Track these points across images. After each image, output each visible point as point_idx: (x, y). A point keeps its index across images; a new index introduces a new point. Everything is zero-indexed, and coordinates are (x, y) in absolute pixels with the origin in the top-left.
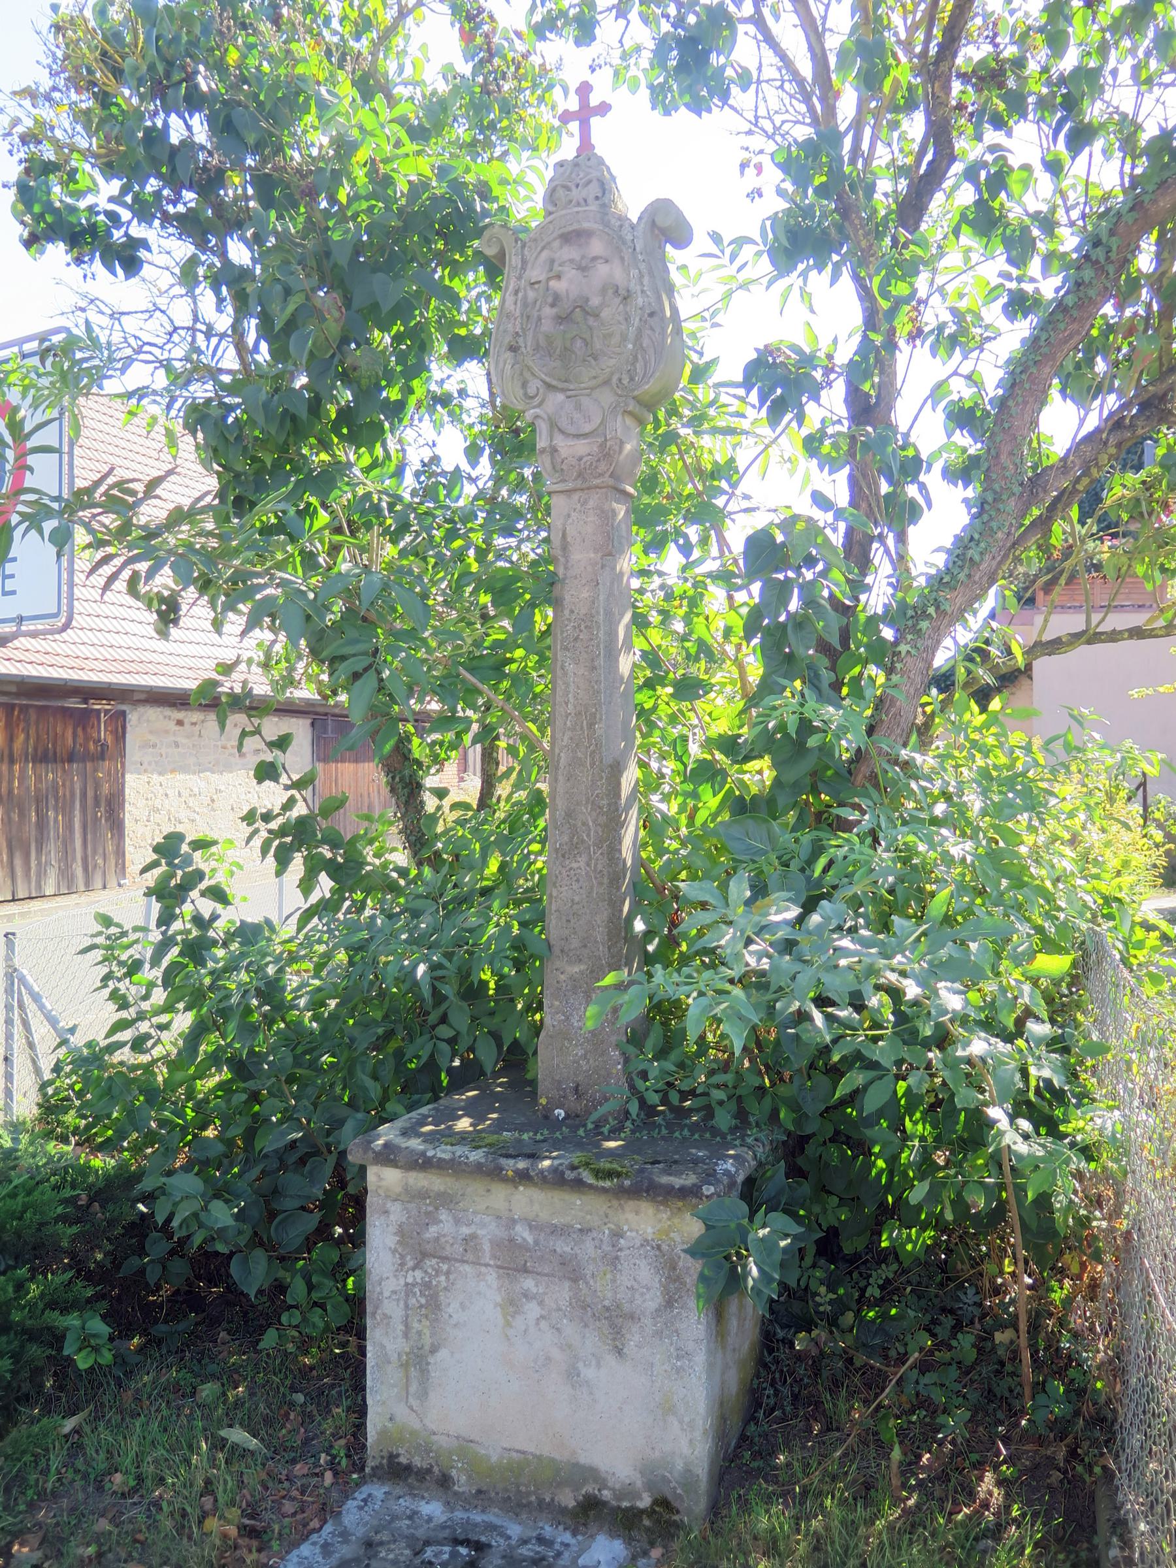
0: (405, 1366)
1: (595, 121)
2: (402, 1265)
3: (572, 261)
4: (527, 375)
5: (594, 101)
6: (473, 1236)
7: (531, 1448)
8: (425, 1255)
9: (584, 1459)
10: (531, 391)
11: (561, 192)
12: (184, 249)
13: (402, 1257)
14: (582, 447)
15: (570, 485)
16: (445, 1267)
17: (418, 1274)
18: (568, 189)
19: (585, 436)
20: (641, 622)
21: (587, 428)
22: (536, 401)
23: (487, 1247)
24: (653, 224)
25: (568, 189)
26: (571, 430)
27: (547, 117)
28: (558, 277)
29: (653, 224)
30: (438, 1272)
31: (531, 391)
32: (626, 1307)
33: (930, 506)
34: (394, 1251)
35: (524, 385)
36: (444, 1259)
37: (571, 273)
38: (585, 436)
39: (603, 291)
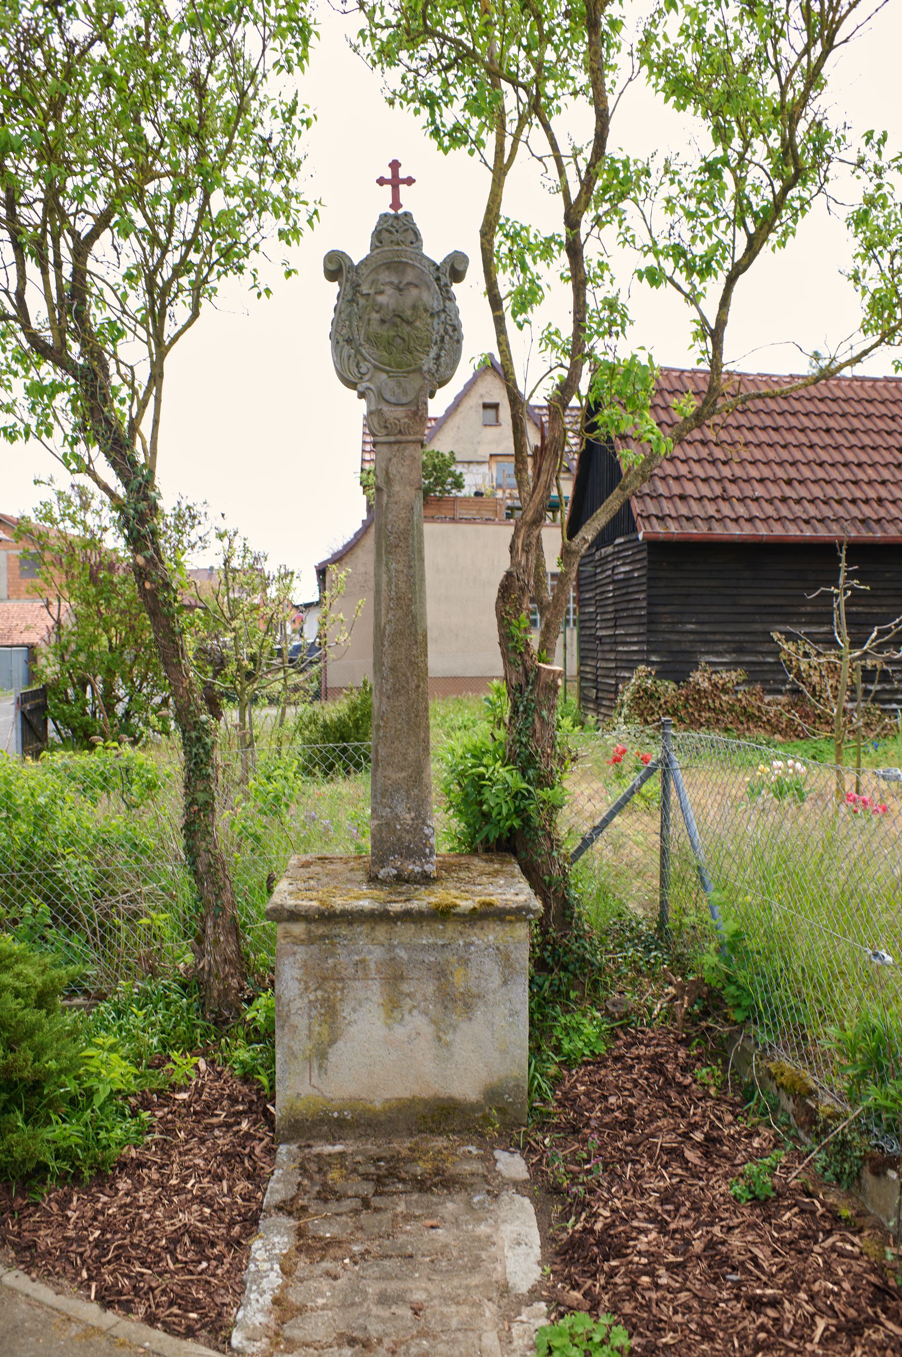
0: (309, 1059)
1: (402, 187)
2: (306, 989)
3: (391, 283)
5: (403, 174)
6: (363, 961)
7: (407, 1095)
8: (325, 979)
9: (444, 1093)
10: (363, 370)
11: (385, 235)
13: (306, 982)
14: (400, 412)
15: (392, 439)
16: (340, 985)
17: (319, 993)
18: (390, 232)
21: (404, 400)
22: (367, 377)
23: (372, 966)
24: (452, 267)
25: (390, 232)
28: (382, 293)
29: (452, 267)
30: (335, 989)
31: (363, 370)
32: (475, 990)
34: (299, 981)
35: (358, 366)
36: (342, 980)
37: (389, 291)
39: (414, 307)
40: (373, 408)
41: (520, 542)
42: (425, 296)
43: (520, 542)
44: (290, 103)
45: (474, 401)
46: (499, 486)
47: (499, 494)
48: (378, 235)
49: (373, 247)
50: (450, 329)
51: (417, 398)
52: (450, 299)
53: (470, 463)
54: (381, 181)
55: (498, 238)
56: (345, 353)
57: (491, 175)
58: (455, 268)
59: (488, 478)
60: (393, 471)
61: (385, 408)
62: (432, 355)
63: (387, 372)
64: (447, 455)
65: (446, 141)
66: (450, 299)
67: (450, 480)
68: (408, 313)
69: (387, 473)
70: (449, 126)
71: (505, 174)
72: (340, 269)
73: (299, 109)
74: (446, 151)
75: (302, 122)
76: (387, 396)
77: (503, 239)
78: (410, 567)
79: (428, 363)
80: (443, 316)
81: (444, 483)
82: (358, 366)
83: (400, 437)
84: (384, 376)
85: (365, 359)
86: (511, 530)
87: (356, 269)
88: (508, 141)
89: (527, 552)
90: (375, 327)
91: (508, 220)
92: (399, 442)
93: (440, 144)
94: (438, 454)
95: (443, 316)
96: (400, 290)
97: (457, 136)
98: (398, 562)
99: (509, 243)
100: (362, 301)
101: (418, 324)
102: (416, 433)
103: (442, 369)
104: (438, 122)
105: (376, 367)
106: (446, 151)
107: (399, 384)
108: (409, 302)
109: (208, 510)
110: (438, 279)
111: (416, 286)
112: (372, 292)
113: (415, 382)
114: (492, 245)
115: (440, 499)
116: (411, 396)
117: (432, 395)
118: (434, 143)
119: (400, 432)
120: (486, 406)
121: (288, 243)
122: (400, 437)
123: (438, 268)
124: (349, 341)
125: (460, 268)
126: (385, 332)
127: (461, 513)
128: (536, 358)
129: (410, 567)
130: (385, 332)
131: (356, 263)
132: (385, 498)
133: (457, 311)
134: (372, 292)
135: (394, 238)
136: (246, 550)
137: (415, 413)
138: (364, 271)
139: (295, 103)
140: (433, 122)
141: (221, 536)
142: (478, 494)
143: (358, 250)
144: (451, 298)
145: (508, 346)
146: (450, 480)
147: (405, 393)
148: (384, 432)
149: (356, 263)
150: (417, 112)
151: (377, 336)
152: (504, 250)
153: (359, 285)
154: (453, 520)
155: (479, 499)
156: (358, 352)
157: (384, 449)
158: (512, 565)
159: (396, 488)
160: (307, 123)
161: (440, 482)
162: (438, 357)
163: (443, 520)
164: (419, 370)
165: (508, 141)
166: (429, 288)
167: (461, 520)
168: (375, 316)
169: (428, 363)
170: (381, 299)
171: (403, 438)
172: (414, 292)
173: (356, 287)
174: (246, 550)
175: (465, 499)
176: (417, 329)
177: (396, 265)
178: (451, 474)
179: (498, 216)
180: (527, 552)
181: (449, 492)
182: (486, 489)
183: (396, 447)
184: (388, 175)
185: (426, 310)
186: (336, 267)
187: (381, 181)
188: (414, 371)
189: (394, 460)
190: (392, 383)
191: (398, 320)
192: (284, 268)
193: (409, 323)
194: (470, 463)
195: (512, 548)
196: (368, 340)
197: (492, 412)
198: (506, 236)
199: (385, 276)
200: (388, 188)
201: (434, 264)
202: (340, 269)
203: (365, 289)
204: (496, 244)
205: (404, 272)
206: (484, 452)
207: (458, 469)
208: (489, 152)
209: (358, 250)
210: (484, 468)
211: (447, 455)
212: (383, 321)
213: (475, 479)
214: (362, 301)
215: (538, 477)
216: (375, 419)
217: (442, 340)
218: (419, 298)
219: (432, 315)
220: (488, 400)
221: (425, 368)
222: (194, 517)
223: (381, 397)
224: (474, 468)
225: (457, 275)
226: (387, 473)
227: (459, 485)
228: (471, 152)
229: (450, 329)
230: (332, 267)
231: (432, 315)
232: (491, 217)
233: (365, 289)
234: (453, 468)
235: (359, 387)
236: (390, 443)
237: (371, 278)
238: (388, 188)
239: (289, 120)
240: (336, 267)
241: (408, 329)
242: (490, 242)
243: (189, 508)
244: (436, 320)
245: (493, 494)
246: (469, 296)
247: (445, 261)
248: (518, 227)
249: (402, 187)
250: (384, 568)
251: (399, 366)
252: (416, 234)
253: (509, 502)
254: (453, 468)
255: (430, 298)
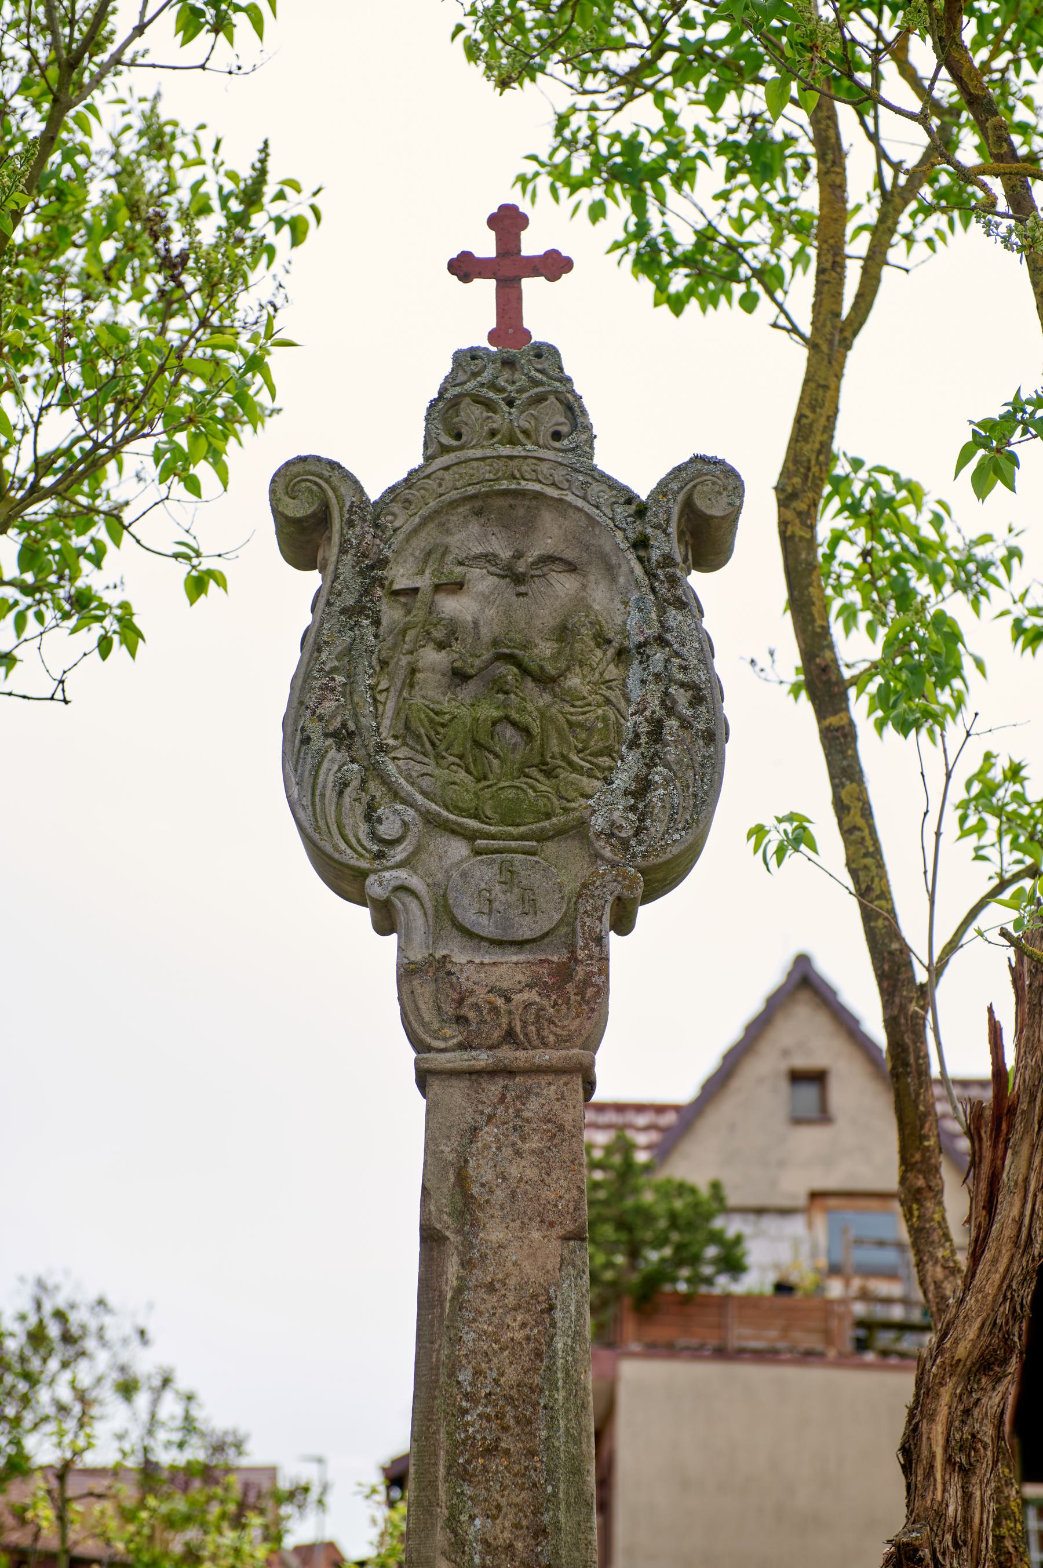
1: (532, 287)
3: (489, 558)
4: (375, 788)
10: (388, 829)
12: (224, 223)
14: (509, 969)
15: (482, 1059)
18: (489, 405)
19: (520, 944)
20: (839, 589)
22: (399, 853)
24: (689, 507)
25: (489, 405)
26: (486, 926)
27: (67, 170)
28: (458, 586)
29: (689, 507)
31: (388, 829)
33: (949, 514)
35: (370, 815)
38: (520, 944)
39: (563, 633)
40: (418, 955)
41: (936, 1433)
42: (600, 597)
43: (936, 1433)
44: (246, 173)
45: (768, 1064)
46: (835, 1270)
47: (835, 1289)
48: (446, 414)
49: (433, 449)
50: (682, 697)
51: (568, 920)
52: (681, 605)
53: (760, 1211)
54: (464, 267)
55: (829, 521)
56: (328, 775)
57: (802, 353)
58: (696, 515)
59: (805, 1249)
60: (480, 1170)
61: (460, 956)
62: (622, 780)
63: (471, 836)
64: (704, 1191)
65: (679, 281)
66: (681, 605)
67: (711, 1251)
68: (545, 649)
69: (462, 1179)
70: (686, 240)
71: (847, 345)
72: (322, 519)
73: (270, 190)
74: (677, 305)
75: (279, 222)
76: (469, 915)
77: (843, 522)
78: (540, 1532)
79: (606, 808)
80: (658, 656)
81: (695, 1260)
82: (370, 815)
83: (507, 1054)
84: (458, 849)
85: (396, 795)
86: (903, 1385)
87: (375, 515)
88: (853, 273)
89: (966, 1472)
90: (431, 690)
91: (857, 464)
92: (510, 1072)
93: (661, 287)
94: (683, 1189)
95: (658, 656)
96: (519, 579)
97: (710, 270)
98: (494, 1513)
99: (861, 536)
100: (391, 614)
101: (574, 681)
102: (562, 1042)
103: (656, 828)
104: (656, 230)
105: (431, 821)
106: (677, 305)
107: (509, 877)
108: (546, 616)
109: (108, 1320)
110: (641, 544)
111: (572, 568)
112: (424, 582)
113: (566, 868)
114: (811, 543)
115: (686, 1300)
116: (550, 915)
117: (624, 924)
118: (647, 286)
119: (510, 1036)
120: (797, 1077)
121: (193, 486)
122: (507, 1054)
123: (641, 511)
124: (344, 737)
125: (716, 510)
126: (467, 707)
127: (742, 1335)
128: (957, 851)
129: (540, 1532)
130: (467, 707)
131: (374, 493)
132: (452, 1268)
133: (706, 649)
134: (424, 582)
135: (497, 421)
136: (189, 1425)
137: (564, 973)
138: (402, 520)
139: (261, 175)
140: (643, 227)
141: (127, 1389)
142: (783, 1288)
143: (384, 454)
144: (688, 605)
145: (867, 812)
146: (711, 1251)
147: (530, 904)
148: (454, 1034)
149: (374, 493)
150: (597, 212)
151: (438, 722)
152: (848, 553)
153: (383, 563)
154: (722, 1353)
155: (784, 1300)
156: (373, 770)
157: (456, 1093)
158: (914, 1517)
159: (495, 1234)
160: (298, 230)
161: (686, 1256)
162: (642, 788)
163: (695, 1353)
164: (579, 829)
165: (853, 273)
166: (610, 571)
167: (740, 1355)
168: (431, 657)
169: (606, 808)
170: (453, 606)
171: (521, 1057)
172: (564, 585)
173: (372, 569)
174: (189, 1425)
175: (750, 1301)
176: (571, 697)
177: (503, 504)
178: (716, 1238)
179: (826, 454)
180: (966, 1472)
181: (709, 1281)
182: (803, 1276)
183: (493, 1088)
184: (486, 246)
185: (602, 640)
186: (312, 511)
187: (464, 267)
188: (560, 833)
189: (488, 1134)
190: (484, 873)
191: (510, 672)
192: (182, 569)
193: (545, 680)
194: (760, 1211)
195: (910, 1454)
196: (407, 732)
197: (809, 1093)
198: (853, 509)
199: (468, 538)
200: (486, 288)
201: (630, 498)
202: (322, 519)
203: (401, 575)
204: (824, 530)
205: (530, 525)
206: (795, 1186)
207: (731, 1226)
208: (801, 292)
209: (384, 454)
210: (796, 1226)
211: (704, 1191)
212: (459, 676)
213: (772, 1253)
214: (391, 614)
215: (990, 1206)
216: (425, 991)
217: (656, 733)
218: (581, 603)
219: (622, 655)
220: (801, 1062)
221: (598, 822)
222: (67, 1338)
223: (445, 917)
224: (770, 1224)
225: (707, 539)
226: (462, 1179)
227: (732, 1263)
228: (749, 303)
229: (682, 697)
230: (299, 509)
231: (622, 655)
232: (808, 449)
233: (401, 575)
234: (718, 1223)
235: (374, 887)
236: (473, 1074)
237: (421, 542)
238: (486, 288)
239: (241, 220)
240: (312, 511)
241: (537, 699)
242: (809, 519)
243: (60, 1315)
244: (635, 671)
245: (820, 1288)
246: (741, 605)
247: (662, 488)
248: (887, 484)
249: (532, 287)
250: (441, 1537)
251: (510, 816)
252: (573, 409)
253: (859, 1309)
254: (718, 1223)
255: (613, 603)
